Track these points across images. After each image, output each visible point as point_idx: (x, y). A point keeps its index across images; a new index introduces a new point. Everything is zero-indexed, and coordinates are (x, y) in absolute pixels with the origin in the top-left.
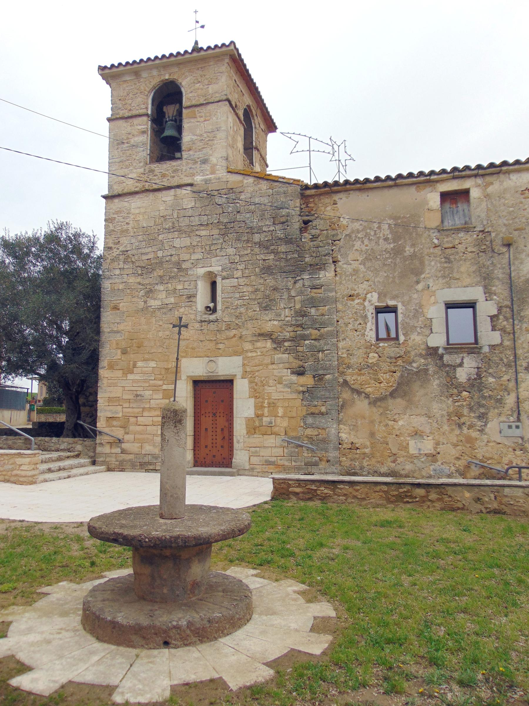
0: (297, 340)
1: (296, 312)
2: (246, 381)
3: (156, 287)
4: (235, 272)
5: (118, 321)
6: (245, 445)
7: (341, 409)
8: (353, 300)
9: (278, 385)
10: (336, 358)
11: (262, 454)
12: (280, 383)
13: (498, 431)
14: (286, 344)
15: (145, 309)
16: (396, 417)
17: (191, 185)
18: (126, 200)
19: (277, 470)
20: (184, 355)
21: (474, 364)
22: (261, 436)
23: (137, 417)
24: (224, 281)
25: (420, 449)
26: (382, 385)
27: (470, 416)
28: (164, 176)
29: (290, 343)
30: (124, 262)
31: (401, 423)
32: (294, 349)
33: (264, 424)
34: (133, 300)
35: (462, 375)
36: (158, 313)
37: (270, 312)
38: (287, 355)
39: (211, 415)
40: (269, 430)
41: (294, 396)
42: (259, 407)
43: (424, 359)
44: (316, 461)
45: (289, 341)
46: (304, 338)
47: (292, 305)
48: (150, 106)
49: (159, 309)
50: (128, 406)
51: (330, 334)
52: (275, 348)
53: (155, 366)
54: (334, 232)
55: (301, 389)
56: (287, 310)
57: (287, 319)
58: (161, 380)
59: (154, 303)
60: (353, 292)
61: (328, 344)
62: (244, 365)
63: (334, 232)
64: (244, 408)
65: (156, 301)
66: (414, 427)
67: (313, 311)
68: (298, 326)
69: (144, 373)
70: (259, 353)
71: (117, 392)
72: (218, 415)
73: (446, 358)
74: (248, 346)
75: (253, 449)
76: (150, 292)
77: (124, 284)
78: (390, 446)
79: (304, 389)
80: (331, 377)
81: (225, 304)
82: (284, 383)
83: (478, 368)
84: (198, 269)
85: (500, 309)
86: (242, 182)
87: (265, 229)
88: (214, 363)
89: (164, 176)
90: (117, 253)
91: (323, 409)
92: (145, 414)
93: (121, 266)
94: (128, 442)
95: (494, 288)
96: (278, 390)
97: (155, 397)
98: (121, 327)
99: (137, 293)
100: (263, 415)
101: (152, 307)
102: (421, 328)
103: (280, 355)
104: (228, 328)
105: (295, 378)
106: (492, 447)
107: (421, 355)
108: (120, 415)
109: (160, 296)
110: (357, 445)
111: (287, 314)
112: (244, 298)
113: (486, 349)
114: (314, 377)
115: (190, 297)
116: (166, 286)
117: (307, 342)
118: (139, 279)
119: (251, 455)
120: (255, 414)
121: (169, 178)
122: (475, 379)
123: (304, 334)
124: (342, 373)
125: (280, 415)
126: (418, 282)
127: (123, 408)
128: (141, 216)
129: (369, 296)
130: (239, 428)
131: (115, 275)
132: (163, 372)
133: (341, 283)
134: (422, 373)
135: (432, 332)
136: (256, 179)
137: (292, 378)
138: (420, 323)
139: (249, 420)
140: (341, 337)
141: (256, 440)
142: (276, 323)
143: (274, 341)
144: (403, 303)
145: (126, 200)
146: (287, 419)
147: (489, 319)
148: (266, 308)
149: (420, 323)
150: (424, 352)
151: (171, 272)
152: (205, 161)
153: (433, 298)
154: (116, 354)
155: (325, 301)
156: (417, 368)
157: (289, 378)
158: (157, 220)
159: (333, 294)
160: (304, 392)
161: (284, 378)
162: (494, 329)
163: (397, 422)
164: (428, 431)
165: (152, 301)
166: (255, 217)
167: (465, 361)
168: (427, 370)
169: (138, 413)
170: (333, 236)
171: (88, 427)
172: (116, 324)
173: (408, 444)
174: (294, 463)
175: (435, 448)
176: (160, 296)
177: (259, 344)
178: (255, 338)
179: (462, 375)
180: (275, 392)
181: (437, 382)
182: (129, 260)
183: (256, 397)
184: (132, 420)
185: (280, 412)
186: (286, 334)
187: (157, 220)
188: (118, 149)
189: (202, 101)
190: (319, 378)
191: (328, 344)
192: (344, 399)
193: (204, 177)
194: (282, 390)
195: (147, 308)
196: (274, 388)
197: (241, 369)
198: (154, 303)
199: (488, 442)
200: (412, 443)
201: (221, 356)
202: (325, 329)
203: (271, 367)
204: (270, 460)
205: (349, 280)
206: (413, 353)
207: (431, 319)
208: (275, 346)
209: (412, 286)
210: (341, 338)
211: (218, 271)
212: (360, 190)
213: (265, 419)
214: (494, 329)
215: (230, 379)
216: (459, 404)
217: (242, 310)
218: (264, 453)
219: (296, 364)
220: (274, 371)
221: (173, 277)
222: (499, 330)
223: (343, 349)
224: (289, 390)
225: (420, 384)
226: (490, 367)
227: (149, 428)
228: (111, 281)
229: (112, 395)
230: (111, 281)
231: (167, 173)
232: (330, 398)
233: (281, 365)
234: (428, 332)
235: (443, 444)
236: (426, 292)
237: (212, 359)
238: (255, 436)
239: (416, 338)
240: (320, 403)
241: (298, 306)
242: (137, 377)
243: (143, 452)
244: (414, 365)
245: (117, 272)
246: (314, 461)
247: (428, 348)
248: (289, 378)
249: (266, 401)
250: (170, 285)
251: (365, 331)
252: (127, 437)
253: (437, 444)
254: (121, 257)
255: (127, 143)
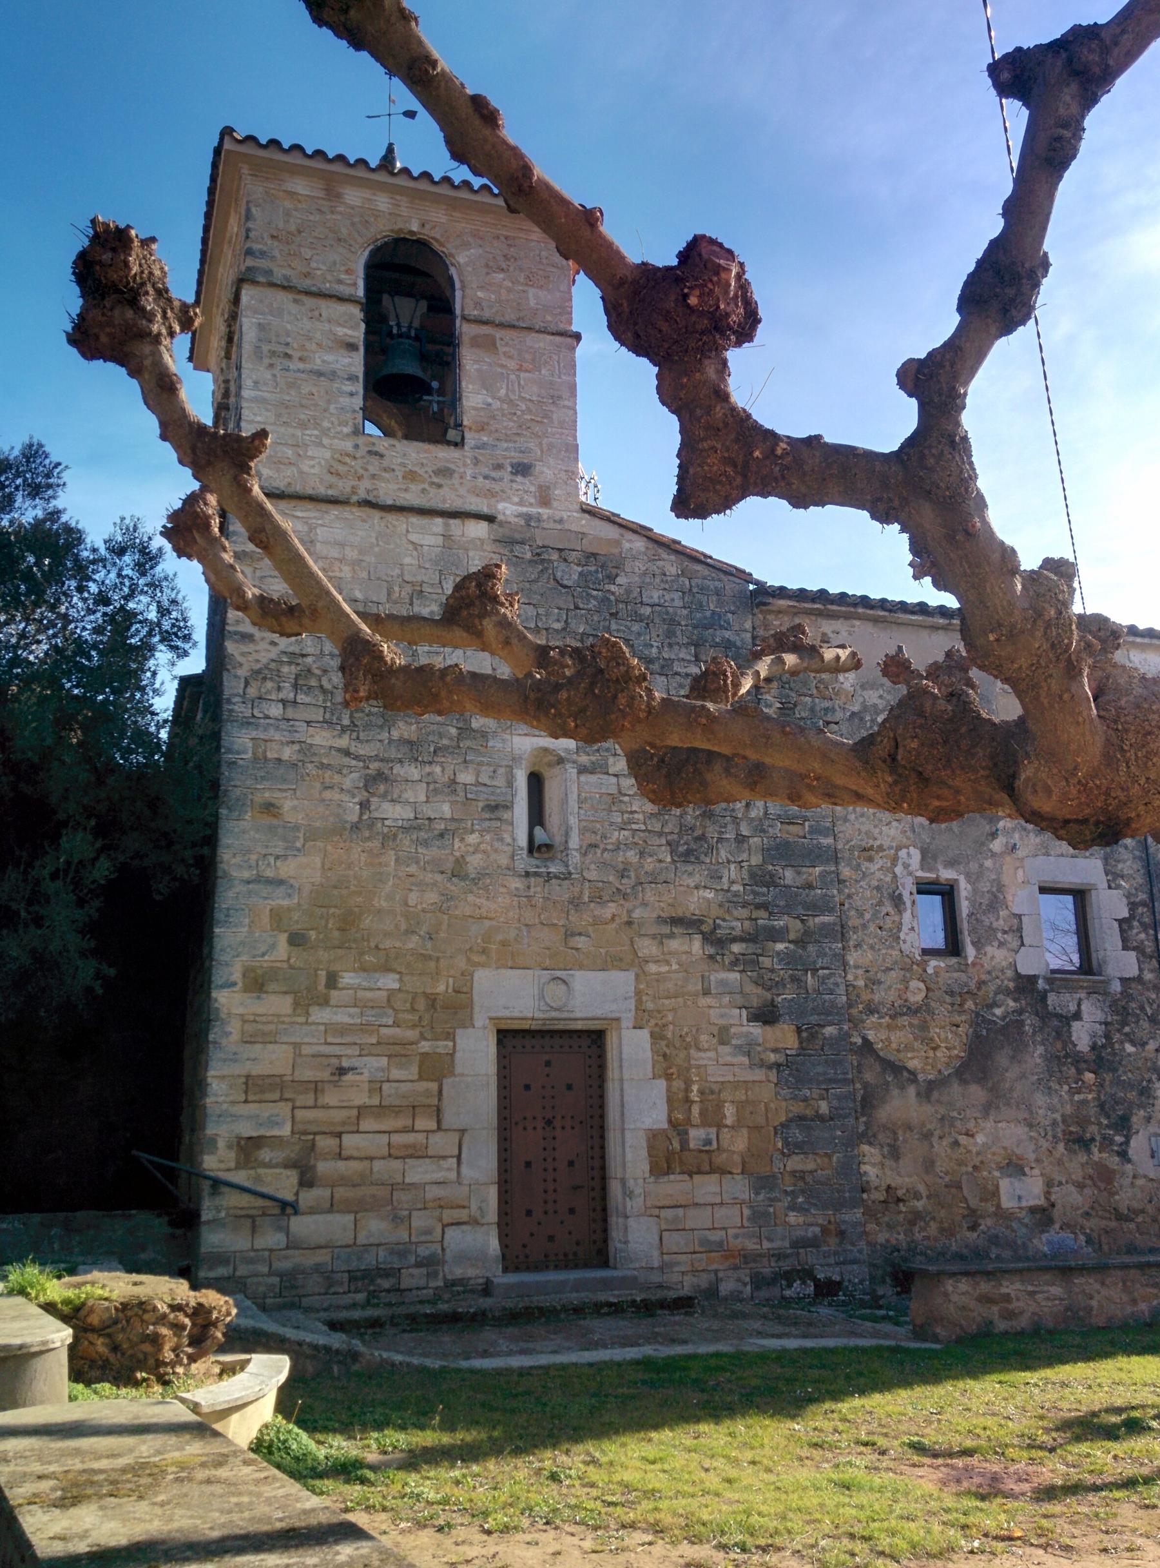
0: (757, 937)
1: (752, 875)
2: (645, 1034)
3: (397, 769)
4: (611, 760)
5: (279, 851)
6: (649, 1204)
7: (863, 1107)
8: (870, 859)
9: (721, 1048)
10: (843, 987)
11: (690, 1224)
12: (722, 1042)
13: (1148, 1153)
14: (736, 948)
15: (363, 826)
16: (971, 1125)
17: (490, 519)
18: (299, 514)
19: (727, 1264)
20: (483, 958)
21: (1100, 1016)
22: (686, 1177)
23: (339, 1135)
24: (583, 778)
25: (1020, 1198)
26: (939, 1054)
27: (1099, 1124)
28: (411, 476)
29: (744, 945)
30: (296, 686)
31: (980, 1139)
32: (752, 961)
33: (692, 1146)
34: (328, 794)
35: (1082, 1036)
36: (405, 841)
37: (697, 868)
38: (738, 975)
39: (540, 1124)
40: (705, 1163)
41: (759, 1075)
42: (677, 1101)
43: (1015, 1000)
44: (815, 1237)
45: (741, 939)
46: (775, 935)
47: (745, 856)
48: (361, 283)
49: (406, 830)
50: (311, 1103)
51: (826, 931)
52: (711, 957)
53: (396, 986)
54: (827, 704)
55: (772, 1057)
56: (732, 867)
57: (735, 888)
58: (414, 1026)
59: (393, 813)
60: (871, 842)
61: (825, 955)
62: (638, 993)
63: (827, 704)
64: (639, 1104)
65: (398, 808)
66: (1005, 1148)
67: (789, 874)
68: (758, 907)
69: (363, 1005)
70: (675, 967)
71: (272, 1060)
72: (558, 1123)
73: (1052, 999)
74: (647, 947)
75: (667, 1214)
76: (377, 781)
77: (296, 747)
78: (965, 1192)
79: (781, 1058)
80: (835, 1032)
81: (588, 835)
82: (734, 1042)
83: (1106, 1024)
84: (516, 739)
85: (1133, 906)
86: (617, 543)
87: (677, 667)
88: (563, 987)
89: (411, 476)
90: (273, 655)
91: (824, 1108)
92: (365, 1125)
93: (288, 693)
94: (312, 1211)
95: (1120, 866)
96: (721, 1061)
97: (396, 1074)
98: (287, 869)
99: (337, 778)
100: (688, 1121)
101: (387, 823)
102: (1005, 932)
103: (723, 975)
104: (598, 899)
105: (759, 1031)
106: (1142, 1188)
107: (1008, 992)
108: (286, 1131)
109: (409, 795)
110: (900, 1193)
111: (733, 876)
112: (634, 826)
113: (1116, 987)
114: (799, 1030)
115: (497, 807)
116: (428, 769)
117: (780, 946)
118: (344, 742)
119: (664, 1227)
120: (670, 1121)
121: (426, 486)
122: (1103, 1046)
123: (773, 927)
124: (856, 1023)
125: (729, 1122)
126: (994, 835)
127: (294, 1108)
128: (346, 569)
129: (903, 853)
130: (629, 1157)
131: (267, 717)
132: (421, 1004)
133: (846, 820)
134: (1011, 1030)
135: (1022, 944)
136: (651, 545)
137: (752, 1030)
138: (1001, 922)
139: (654, 1136)
140: (853, 938)
141: (675, 1186)
142: (710, 895)
143: (708, 938)
144: (968, 876)
145: (299, 514)
146: (745, 1131)
147: (1116, 925)
148: (688, 856)
149: (1001, 922)
150: (1011, 985)
151: (441, 736)
152: (522, 469)
153: (1020, 872)
154: (273, 946)
155: (816, 855)
156: (1003, 1018)
157: (745, 1029)
158: (397, 589)
159: (830, 840)
160: (778, 1065)
161: (733, 1030)
162: (1125, 948)
163: (972, 1136)
164: (1032, 1157)
165: (386, 806)
166: (654, 635)
167: (1083, 1007)
168: (1021, 1023)
169: (344, 1123)
170: (826, 710)
171: (151, 1162)
172: (272, 860)
173: (997, 1187)
174: (766, 1245)
175: (1048, 1194)
176: (409, 795)
177: (674, 944)
178: (666, 930)
179: (1082, 1036)
180: (718, 1065)
181: (1040, 1050)
182: (313, 682)
183: (669, 1077)
184: (325, 1143)
185: (729, 1111)
186: (734, 924)
187: (397, 589)
188: (271, 366)
189: (510, 316)
190: (808, 1034)
191: (825, 955)
192: (866, 1086)
193: (525, 510)
194: (729, 1059)
195: (372, 822)
196: (711, 1054)
197: (632, 1004)
198: (393, 813)
199: (1135, 1177)
200: (1005, 1184)
201: (581, 967)
202: (817, 920)
203: (704, 1001)
204: (713, 1238)
205: (862, 815)
206: (992, 987)
207: (1020, 916)
208: (711, 950)
209: (983, 844)
210: (851, 943)
211: (567, 751)
212: (876, 620)
213: (693, 1133)
214: (1125, 948)
215: (598, 1027)
216: (1082, 1097)
217: (632, 856)
218: (698, 1219)
219: (757, 995)
220: (712, 1011)
221: (446, 748)
222: (1134, 949)
223: (857, 967)
224: (746, 1060)
225: (1011, 1053)
226: (1124, 1023)
227: (378, 1165)
228: (254, 734)
229: (256, 1070)
230: (254, 734)
231: (421, 471)
232: (836, 1081)
233: (726, 999)
234: (1015, 944)
235: (1060, 1183)
236: (1008, 858)
237: (558, 973)
238: (672, 1177)
239: (997, 956)
240: (816, 1093)
241: (756, 860)
242: (342, 1017)
243: (362, 1239)
244: (998, 1011)
245: (276, 711)
246: (810, 1235)
247: (1018, 976)
248: (745, 1029)
249: (695, 1088)
250: (438, 769)
251: (900, 930)
252: (308, 1197)
253: (1049, 1184)
254: (285, 669)
255: (300, 359)
